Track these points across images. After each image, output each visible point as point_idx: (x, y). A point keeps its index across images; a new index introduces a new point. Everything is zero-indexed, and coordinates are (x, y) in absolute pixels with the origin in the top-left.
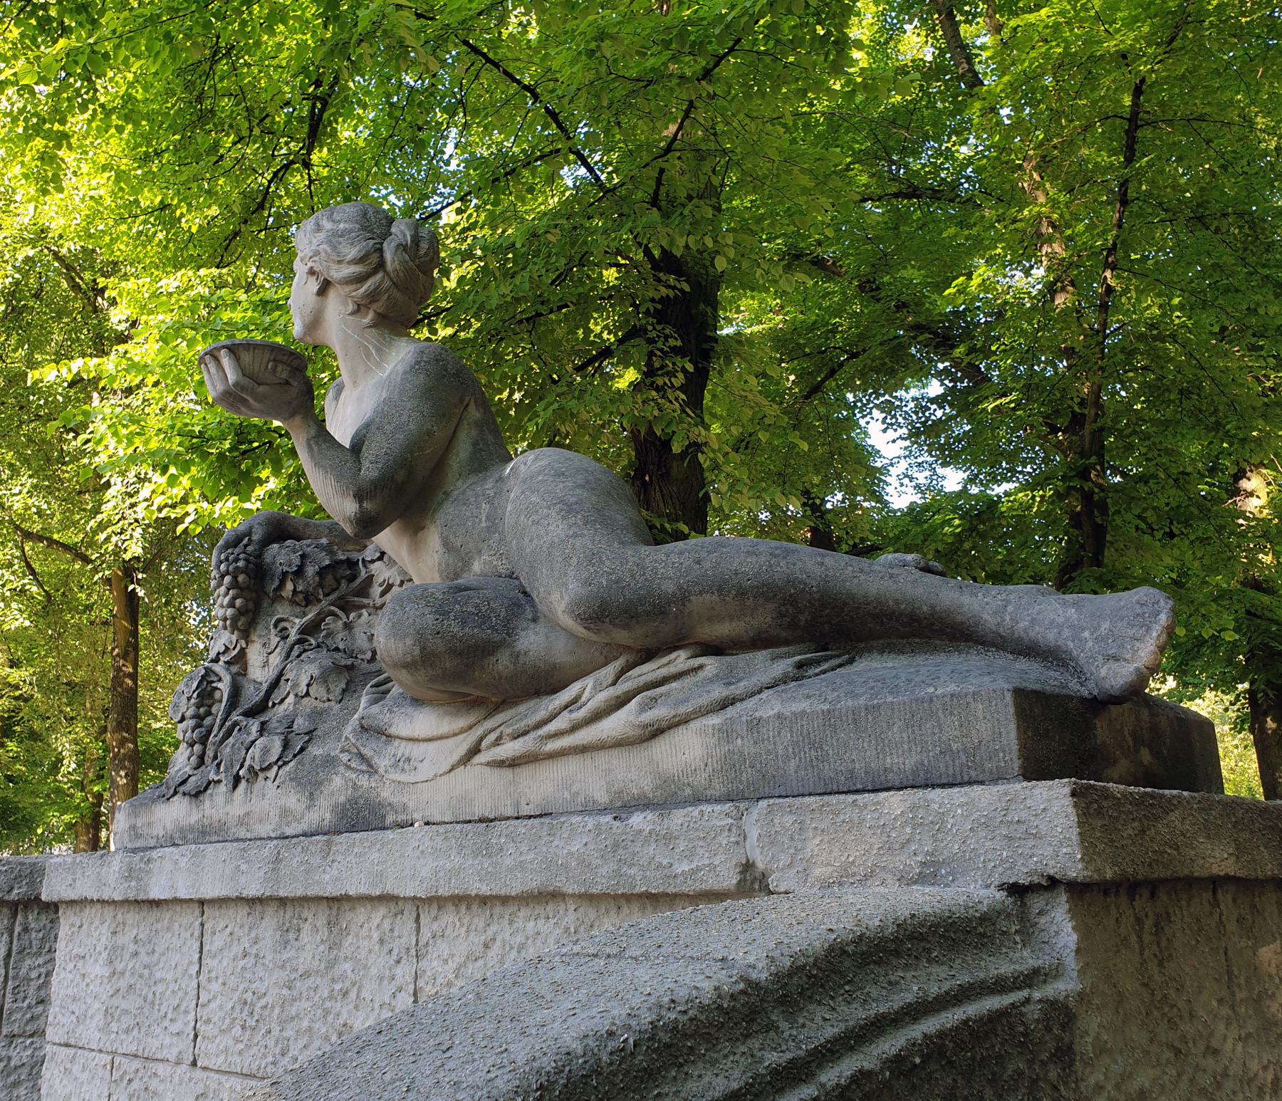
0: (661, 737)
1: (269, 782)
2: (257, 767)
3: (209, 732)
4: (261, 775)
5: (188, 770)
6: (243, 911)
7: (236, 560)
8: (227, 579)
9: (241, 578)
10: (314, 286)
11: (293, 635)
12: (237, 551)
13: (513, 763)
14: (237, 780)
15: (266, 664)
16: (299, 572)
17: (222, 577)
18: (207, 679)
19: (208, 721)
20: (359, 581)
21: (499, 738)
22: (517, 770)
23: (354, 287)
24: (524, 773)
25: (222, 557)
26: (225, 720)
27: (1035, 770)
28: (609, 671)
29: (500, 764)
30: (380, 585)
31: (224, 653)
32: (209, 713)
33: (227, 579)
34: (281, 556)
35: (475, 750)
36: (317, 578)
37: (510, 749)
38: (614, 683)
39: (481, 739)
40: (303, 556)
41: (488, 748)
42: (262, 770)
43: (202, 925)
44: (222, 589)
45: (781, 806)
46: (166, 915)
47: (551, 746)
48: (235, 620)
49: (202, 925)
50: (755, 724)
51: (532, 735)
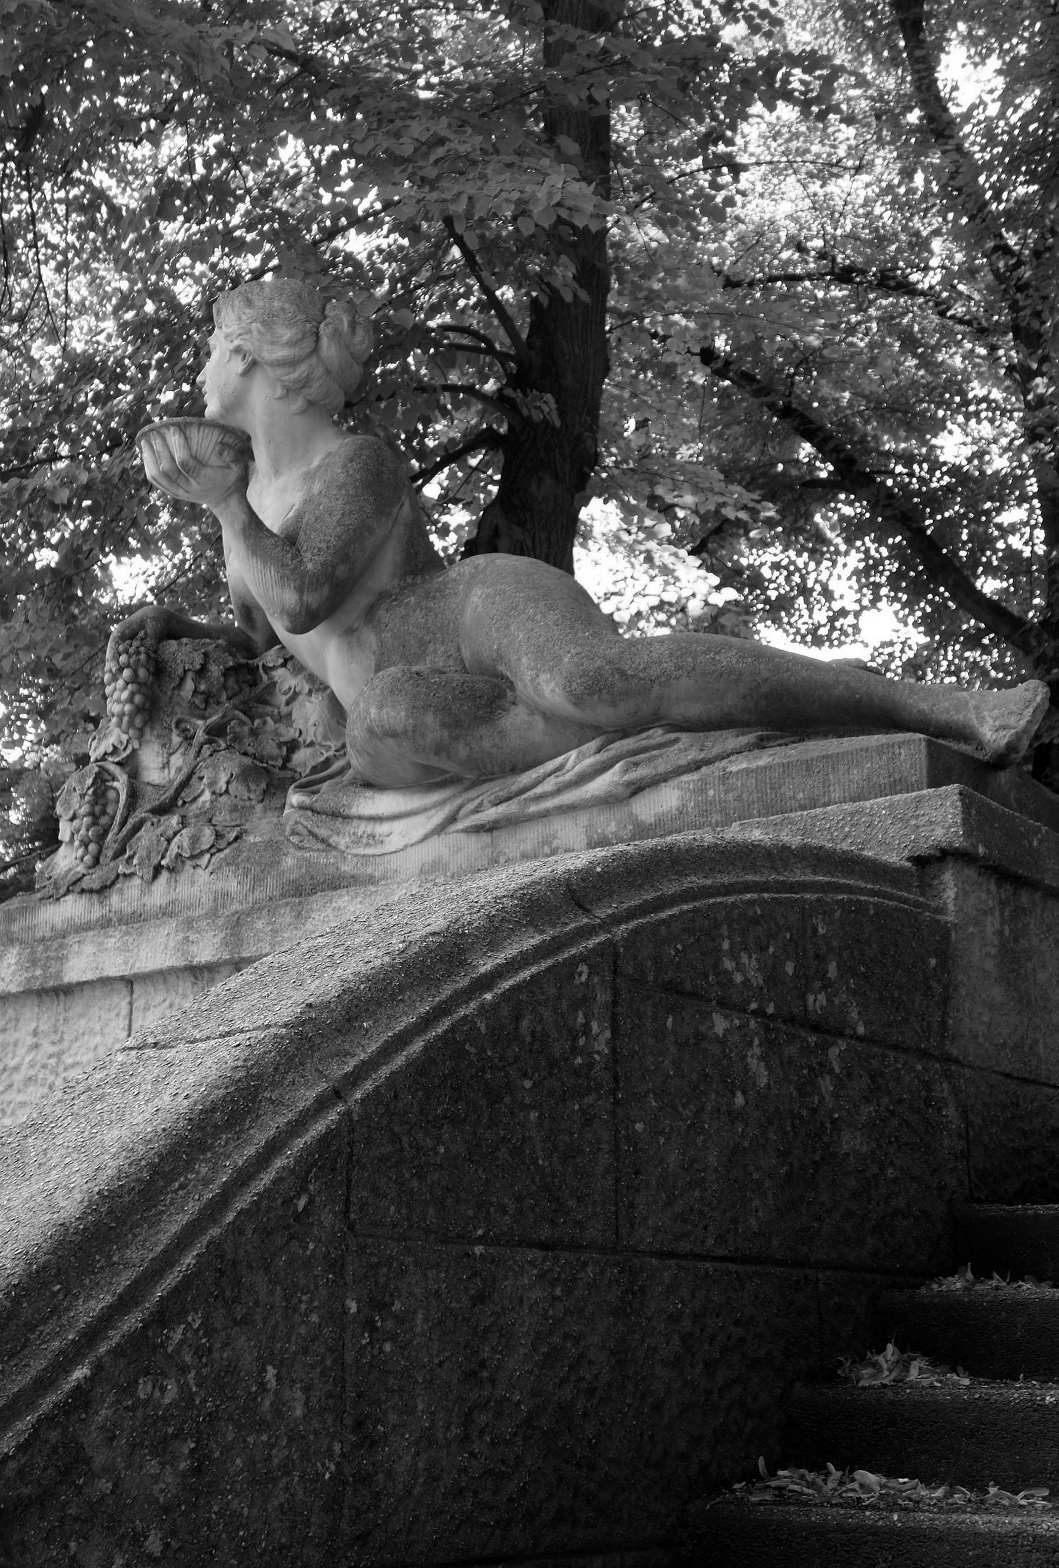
0: (641, 794)
1: (199, 871)
2: (186, 854)
3: (106, 832)
4: (189, 864)
5: (81, 869)
6: (185, 985)
7: (138, 653)
8: (126, 673)
9: (142, 672)
10: (238, 366)
11: (200, 736)
12: (136, 643)
13: (490, 828)
14: (158, 870)
15: (166, 765)
16: (202, 672)
17: (121, 670)
18: (102, 779)
19: (104, 820)
20: (261, 687)
21: (481, 804)
22: (495, 833)
23: (287, 369)
24: (501, 836)
25: (121, 648)
26: (123, 823)
27: (935, 782)
28: (593, 745)
29: (478, 829)
30: (285, 693)
31: (112, 754)
32: (104, 812)
33: (126, 673)
34: (182, 654)
35: (452, 819)
36: (222, 679)
37: (491, 814)
38: (599, 751)
39: (460, 807)
40: (206, 655)
41: (466, 816)
42: (192, 857)
43: (131, 1004)
44: (120, 683)
45: (750, 824)
46: (77, 1005)
47: (533, 808)
48: (132, 716)
49: (131, 1004)
50: (725, 777)
51: (516, 800)
